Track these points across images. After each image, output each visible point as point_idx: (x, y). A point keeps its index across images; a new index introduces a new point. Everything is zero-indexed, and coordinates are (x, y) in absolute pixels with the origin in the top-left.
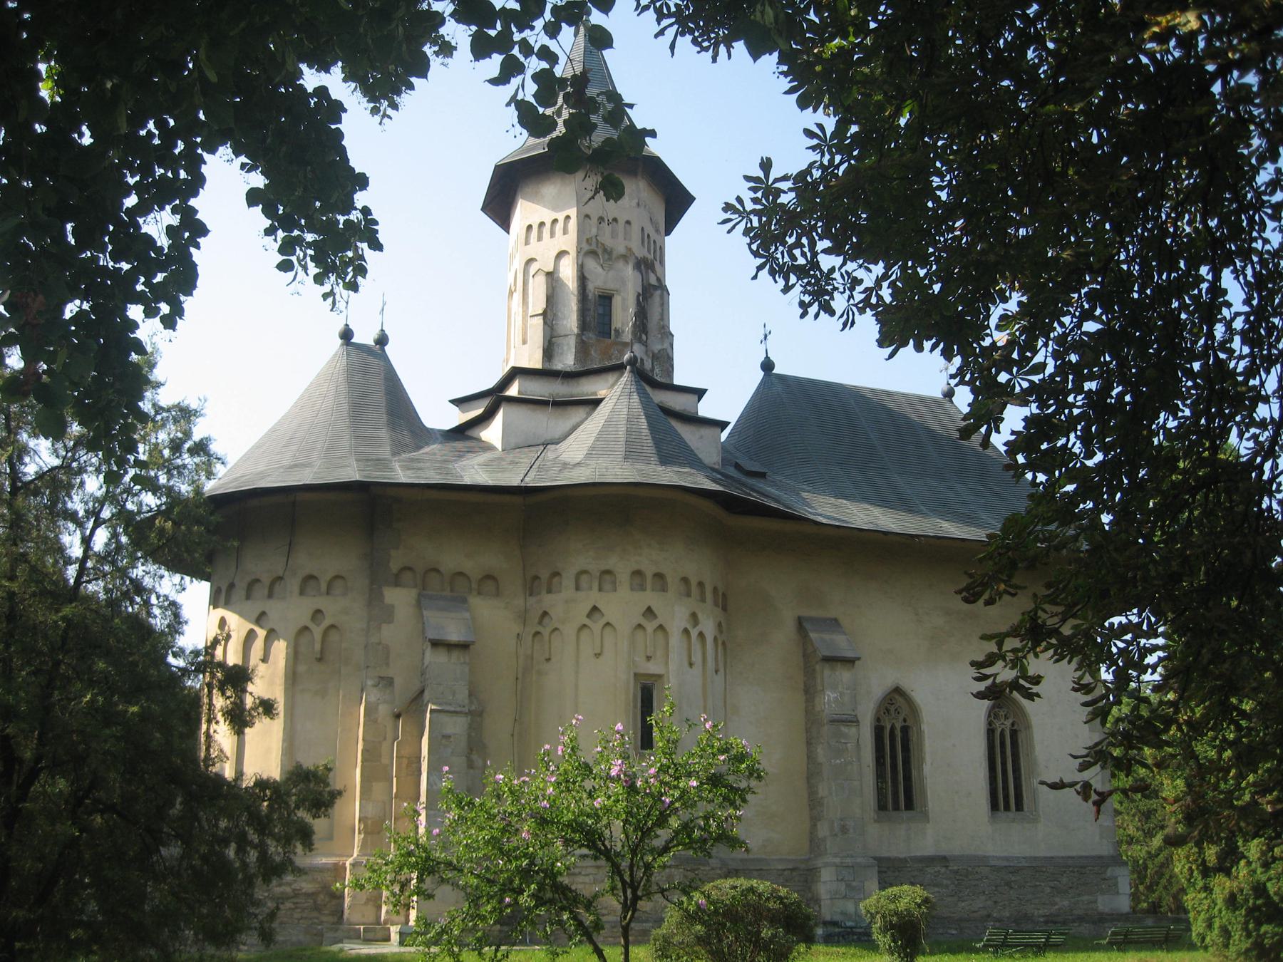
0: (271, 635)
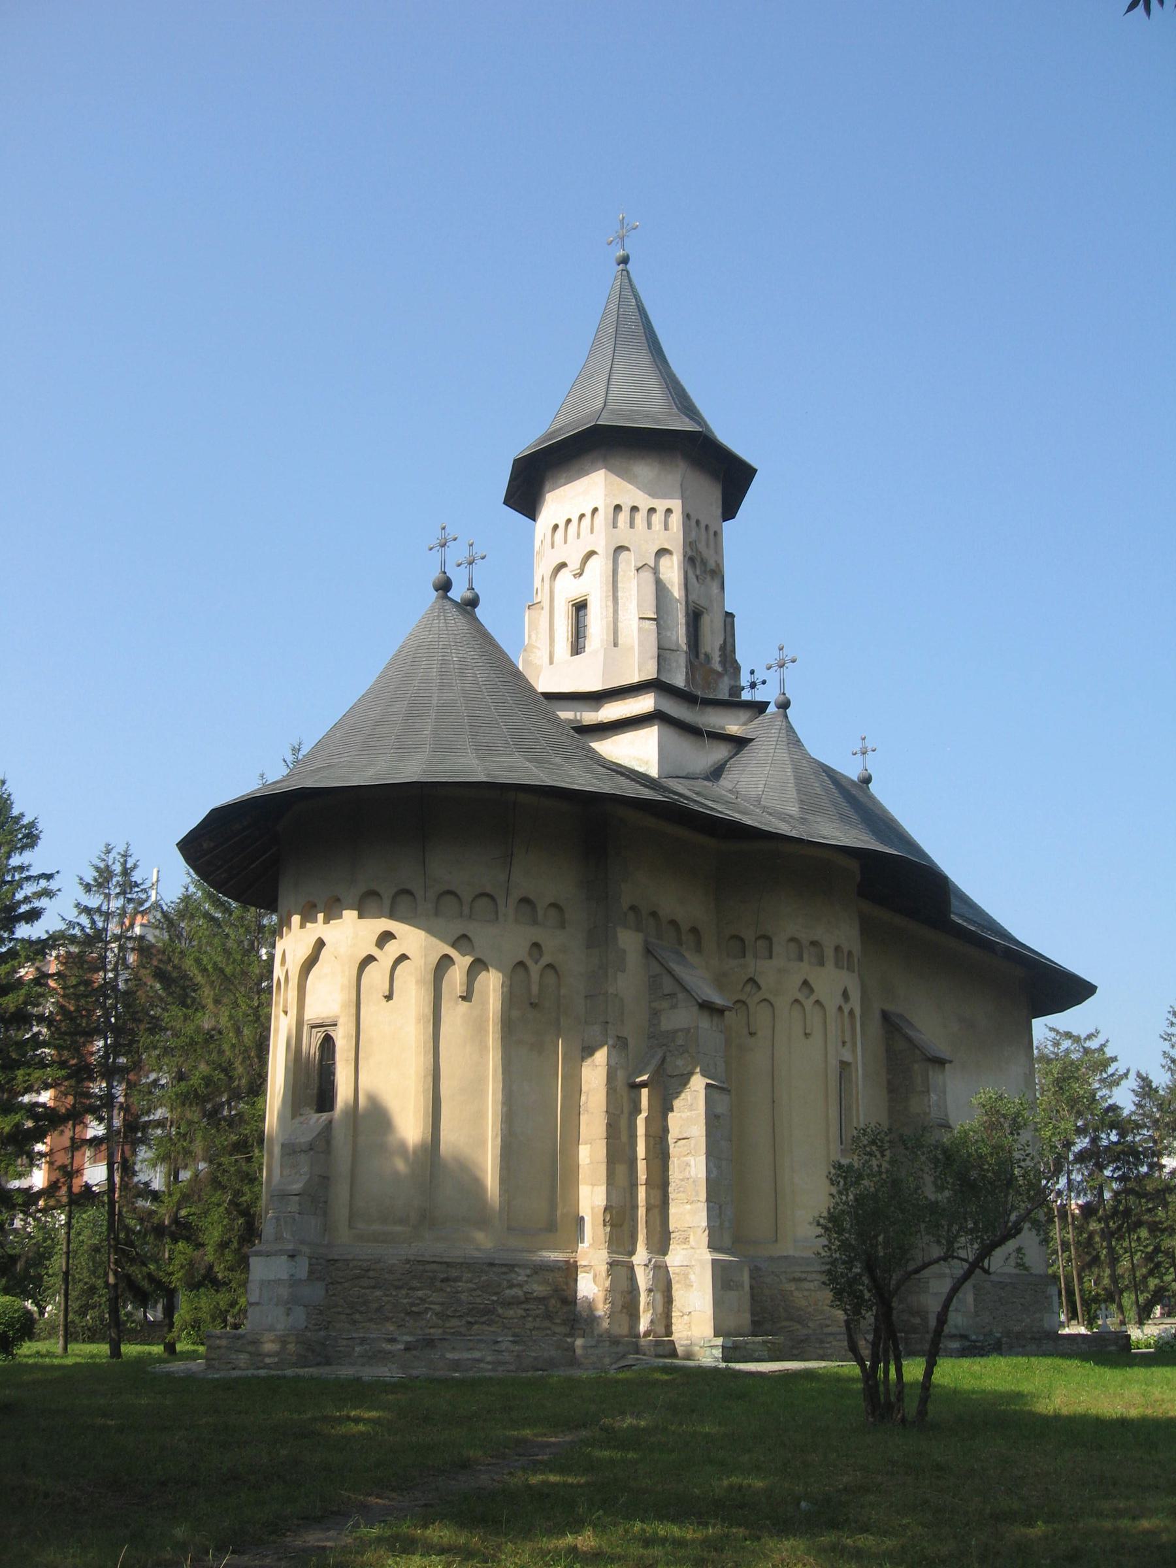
0: (478, 965)
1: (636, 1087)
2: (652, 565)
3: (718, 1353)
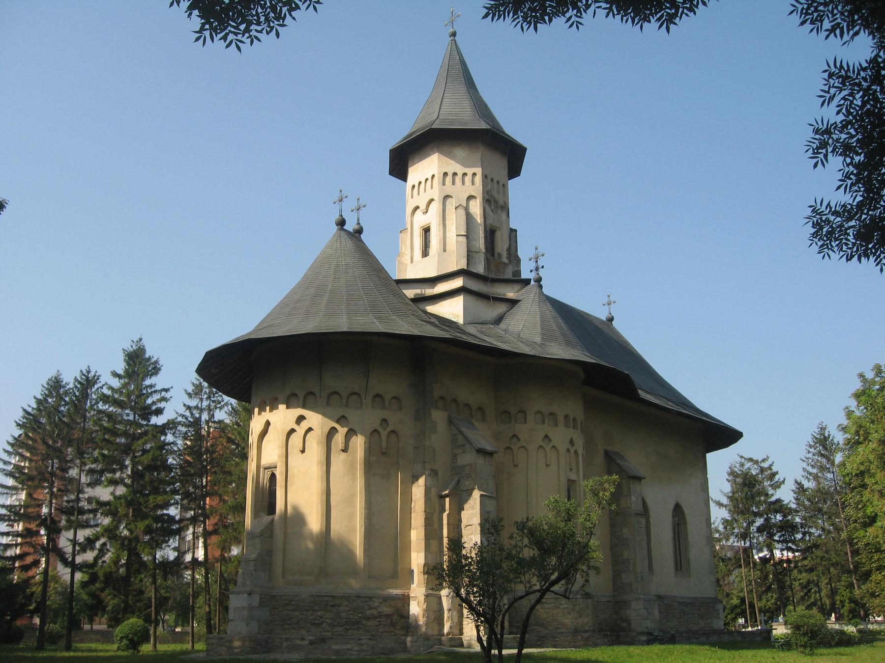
0: (351, 433)
1: (443, 497)
2: (465, 205)
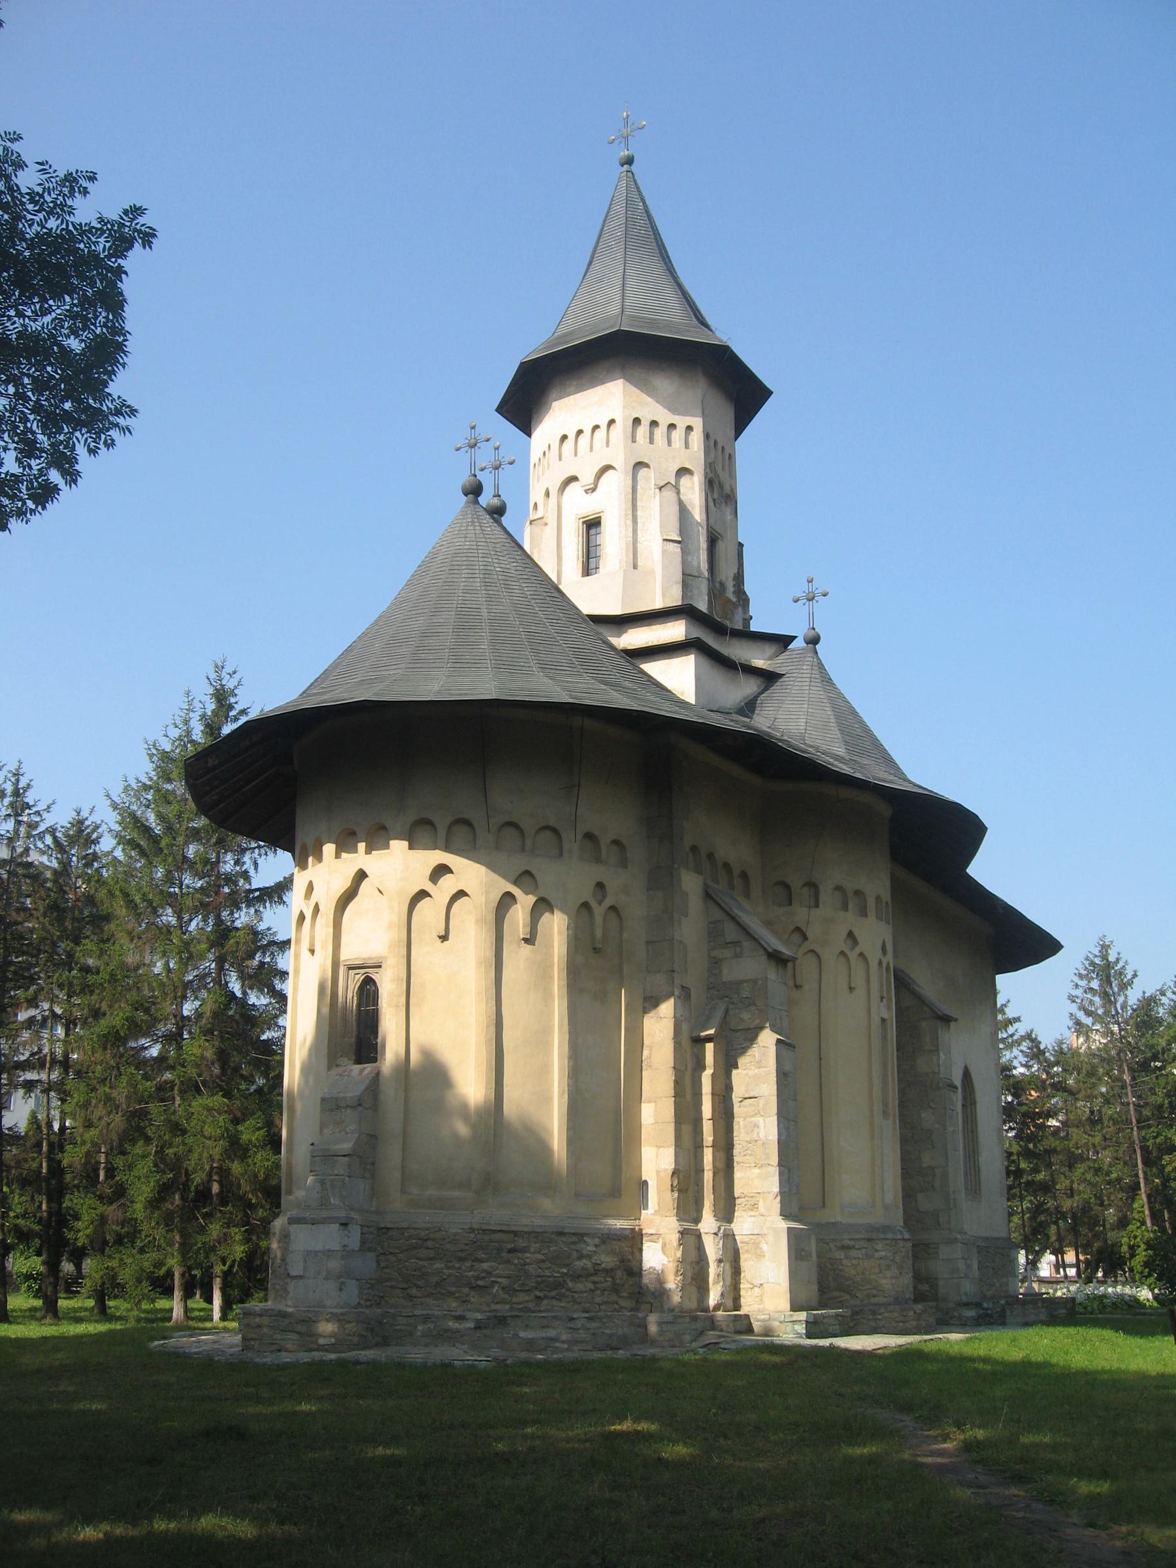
0: (543, 905)
1: (700, 1042)
3: (801, 1328)
